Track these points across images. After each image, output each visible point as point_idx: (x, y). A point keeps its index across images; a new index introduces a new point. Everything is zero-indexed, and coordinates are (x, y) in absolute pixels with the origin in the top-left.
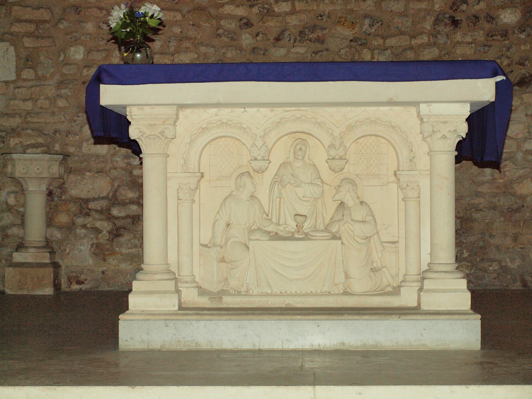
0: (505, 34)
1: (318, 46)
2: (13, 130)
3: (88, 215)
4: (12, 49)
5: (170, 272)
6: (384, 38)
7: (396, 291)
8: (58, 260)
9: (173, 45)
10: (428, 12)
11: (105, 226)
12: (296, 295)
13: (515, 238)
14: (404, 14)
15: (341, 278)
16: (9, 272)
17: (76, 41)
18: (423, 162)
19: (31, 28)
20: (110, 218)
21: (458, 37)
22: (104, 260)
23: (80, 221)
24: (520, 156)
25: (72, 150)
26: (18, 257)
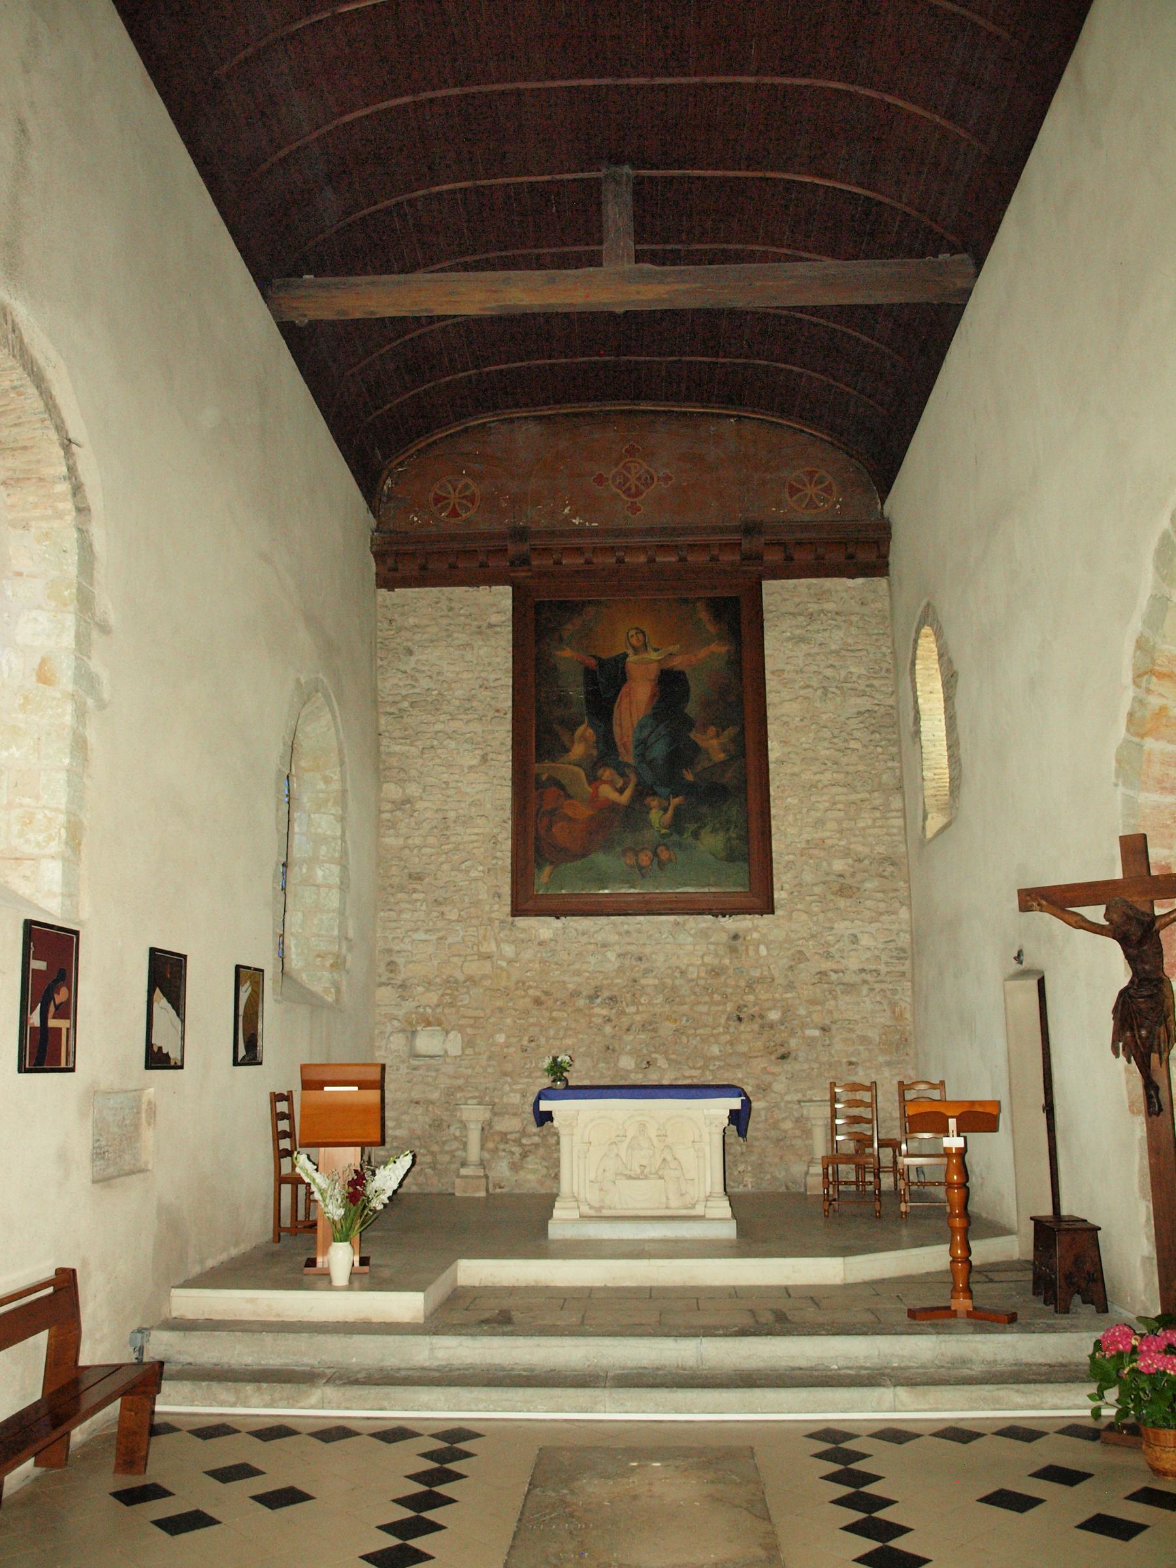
0: (771, 1026)
1: (653, 1034)
2: (459, 1087)
3: (507, 1143)
4: (459, 1035)
5: (574, 1197)
6: (696, 1029)
7: (693, 1207)
8: (487, 1172)
9: (562, 1033)
10: (724, 1012)
11: (517, 1150)
12: (643, 1209)
13: (781, 1158)
14: (708, 1014)
15: (664, 1200)
16: (458, 1181)
17: (500, 1031)
18: (706, 1138)
19: (471, 1021)
20: (521, 1145)
21: (742, 1027)
22: (517, 1172)
23: (501, 1146)
24: (782, 1105)
25: (496, 1100)
26: (463, 1171)
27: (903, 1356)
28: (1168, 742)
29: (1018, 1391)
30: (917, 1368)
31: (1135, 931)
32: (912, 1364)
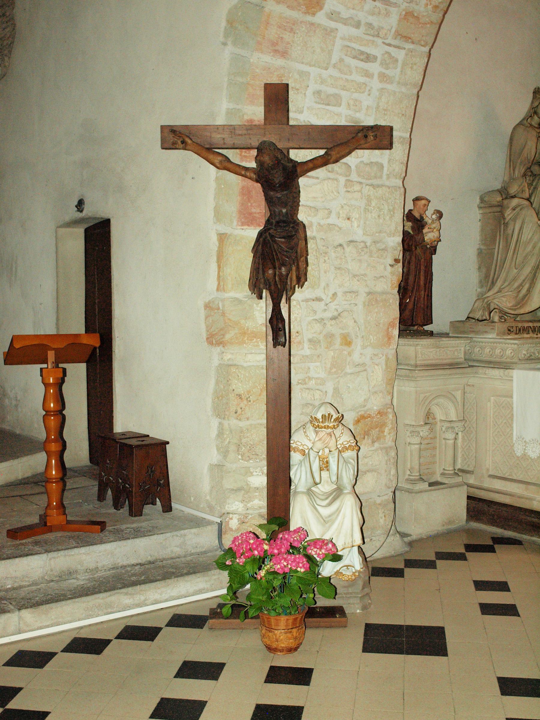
27: (16, 578)
28: (288, 7)
29: (126, 594)
30: (28, 586)
31: (278, 178)
32: (24, 583)
